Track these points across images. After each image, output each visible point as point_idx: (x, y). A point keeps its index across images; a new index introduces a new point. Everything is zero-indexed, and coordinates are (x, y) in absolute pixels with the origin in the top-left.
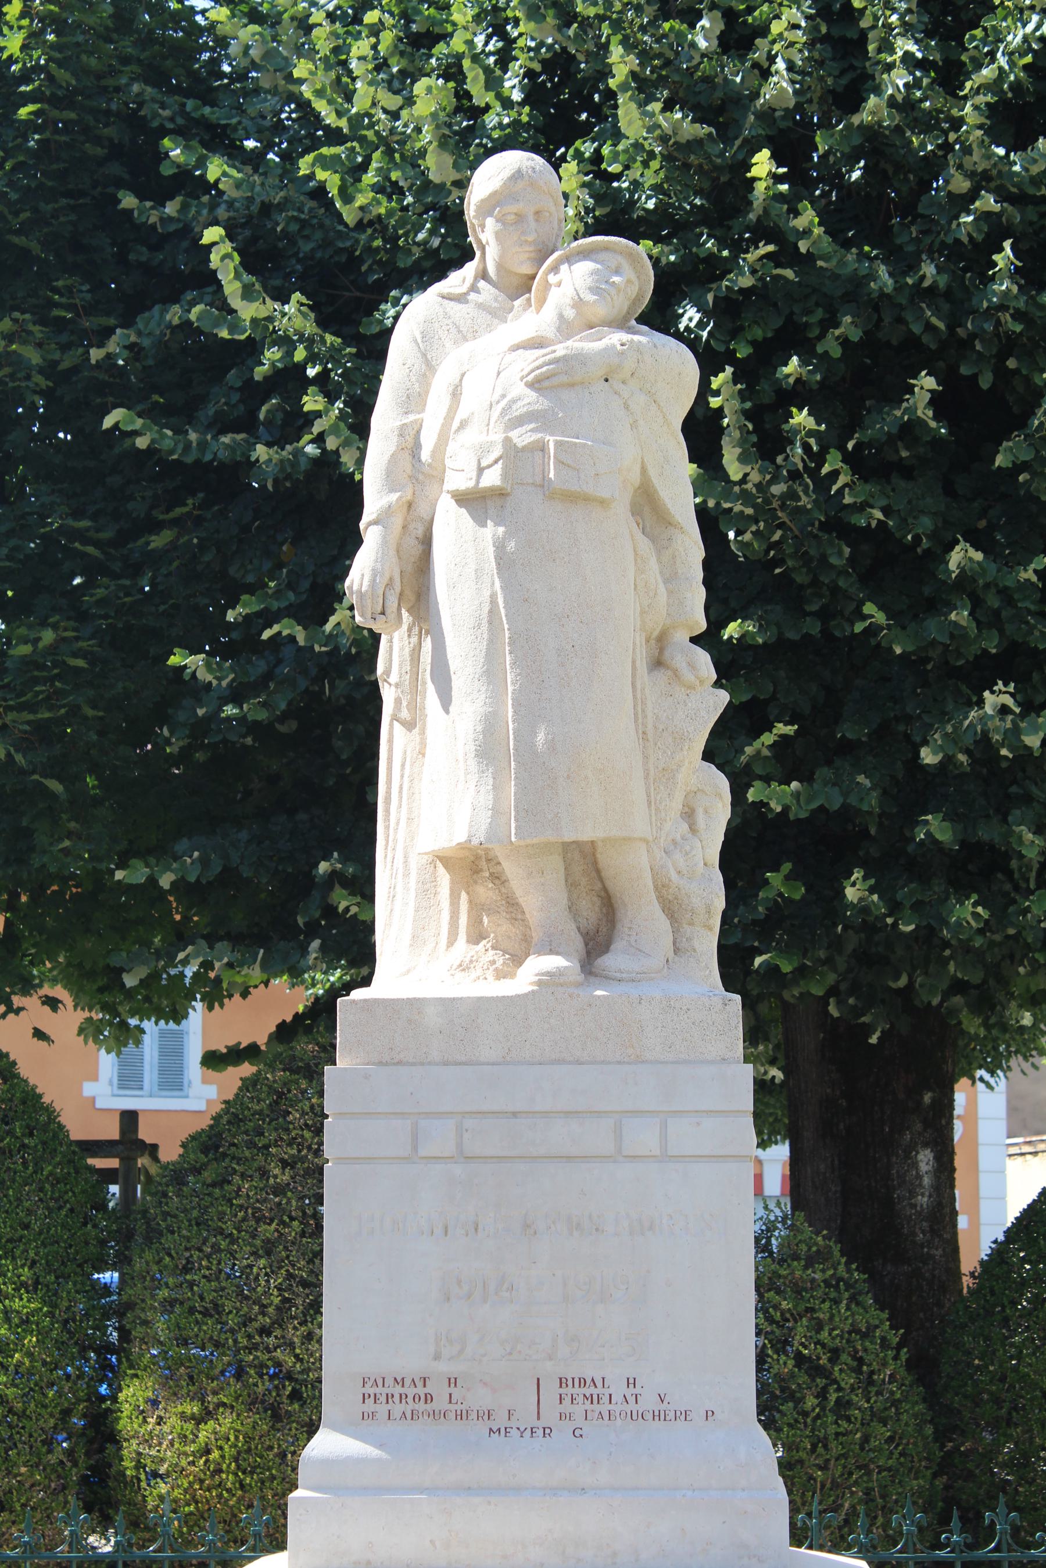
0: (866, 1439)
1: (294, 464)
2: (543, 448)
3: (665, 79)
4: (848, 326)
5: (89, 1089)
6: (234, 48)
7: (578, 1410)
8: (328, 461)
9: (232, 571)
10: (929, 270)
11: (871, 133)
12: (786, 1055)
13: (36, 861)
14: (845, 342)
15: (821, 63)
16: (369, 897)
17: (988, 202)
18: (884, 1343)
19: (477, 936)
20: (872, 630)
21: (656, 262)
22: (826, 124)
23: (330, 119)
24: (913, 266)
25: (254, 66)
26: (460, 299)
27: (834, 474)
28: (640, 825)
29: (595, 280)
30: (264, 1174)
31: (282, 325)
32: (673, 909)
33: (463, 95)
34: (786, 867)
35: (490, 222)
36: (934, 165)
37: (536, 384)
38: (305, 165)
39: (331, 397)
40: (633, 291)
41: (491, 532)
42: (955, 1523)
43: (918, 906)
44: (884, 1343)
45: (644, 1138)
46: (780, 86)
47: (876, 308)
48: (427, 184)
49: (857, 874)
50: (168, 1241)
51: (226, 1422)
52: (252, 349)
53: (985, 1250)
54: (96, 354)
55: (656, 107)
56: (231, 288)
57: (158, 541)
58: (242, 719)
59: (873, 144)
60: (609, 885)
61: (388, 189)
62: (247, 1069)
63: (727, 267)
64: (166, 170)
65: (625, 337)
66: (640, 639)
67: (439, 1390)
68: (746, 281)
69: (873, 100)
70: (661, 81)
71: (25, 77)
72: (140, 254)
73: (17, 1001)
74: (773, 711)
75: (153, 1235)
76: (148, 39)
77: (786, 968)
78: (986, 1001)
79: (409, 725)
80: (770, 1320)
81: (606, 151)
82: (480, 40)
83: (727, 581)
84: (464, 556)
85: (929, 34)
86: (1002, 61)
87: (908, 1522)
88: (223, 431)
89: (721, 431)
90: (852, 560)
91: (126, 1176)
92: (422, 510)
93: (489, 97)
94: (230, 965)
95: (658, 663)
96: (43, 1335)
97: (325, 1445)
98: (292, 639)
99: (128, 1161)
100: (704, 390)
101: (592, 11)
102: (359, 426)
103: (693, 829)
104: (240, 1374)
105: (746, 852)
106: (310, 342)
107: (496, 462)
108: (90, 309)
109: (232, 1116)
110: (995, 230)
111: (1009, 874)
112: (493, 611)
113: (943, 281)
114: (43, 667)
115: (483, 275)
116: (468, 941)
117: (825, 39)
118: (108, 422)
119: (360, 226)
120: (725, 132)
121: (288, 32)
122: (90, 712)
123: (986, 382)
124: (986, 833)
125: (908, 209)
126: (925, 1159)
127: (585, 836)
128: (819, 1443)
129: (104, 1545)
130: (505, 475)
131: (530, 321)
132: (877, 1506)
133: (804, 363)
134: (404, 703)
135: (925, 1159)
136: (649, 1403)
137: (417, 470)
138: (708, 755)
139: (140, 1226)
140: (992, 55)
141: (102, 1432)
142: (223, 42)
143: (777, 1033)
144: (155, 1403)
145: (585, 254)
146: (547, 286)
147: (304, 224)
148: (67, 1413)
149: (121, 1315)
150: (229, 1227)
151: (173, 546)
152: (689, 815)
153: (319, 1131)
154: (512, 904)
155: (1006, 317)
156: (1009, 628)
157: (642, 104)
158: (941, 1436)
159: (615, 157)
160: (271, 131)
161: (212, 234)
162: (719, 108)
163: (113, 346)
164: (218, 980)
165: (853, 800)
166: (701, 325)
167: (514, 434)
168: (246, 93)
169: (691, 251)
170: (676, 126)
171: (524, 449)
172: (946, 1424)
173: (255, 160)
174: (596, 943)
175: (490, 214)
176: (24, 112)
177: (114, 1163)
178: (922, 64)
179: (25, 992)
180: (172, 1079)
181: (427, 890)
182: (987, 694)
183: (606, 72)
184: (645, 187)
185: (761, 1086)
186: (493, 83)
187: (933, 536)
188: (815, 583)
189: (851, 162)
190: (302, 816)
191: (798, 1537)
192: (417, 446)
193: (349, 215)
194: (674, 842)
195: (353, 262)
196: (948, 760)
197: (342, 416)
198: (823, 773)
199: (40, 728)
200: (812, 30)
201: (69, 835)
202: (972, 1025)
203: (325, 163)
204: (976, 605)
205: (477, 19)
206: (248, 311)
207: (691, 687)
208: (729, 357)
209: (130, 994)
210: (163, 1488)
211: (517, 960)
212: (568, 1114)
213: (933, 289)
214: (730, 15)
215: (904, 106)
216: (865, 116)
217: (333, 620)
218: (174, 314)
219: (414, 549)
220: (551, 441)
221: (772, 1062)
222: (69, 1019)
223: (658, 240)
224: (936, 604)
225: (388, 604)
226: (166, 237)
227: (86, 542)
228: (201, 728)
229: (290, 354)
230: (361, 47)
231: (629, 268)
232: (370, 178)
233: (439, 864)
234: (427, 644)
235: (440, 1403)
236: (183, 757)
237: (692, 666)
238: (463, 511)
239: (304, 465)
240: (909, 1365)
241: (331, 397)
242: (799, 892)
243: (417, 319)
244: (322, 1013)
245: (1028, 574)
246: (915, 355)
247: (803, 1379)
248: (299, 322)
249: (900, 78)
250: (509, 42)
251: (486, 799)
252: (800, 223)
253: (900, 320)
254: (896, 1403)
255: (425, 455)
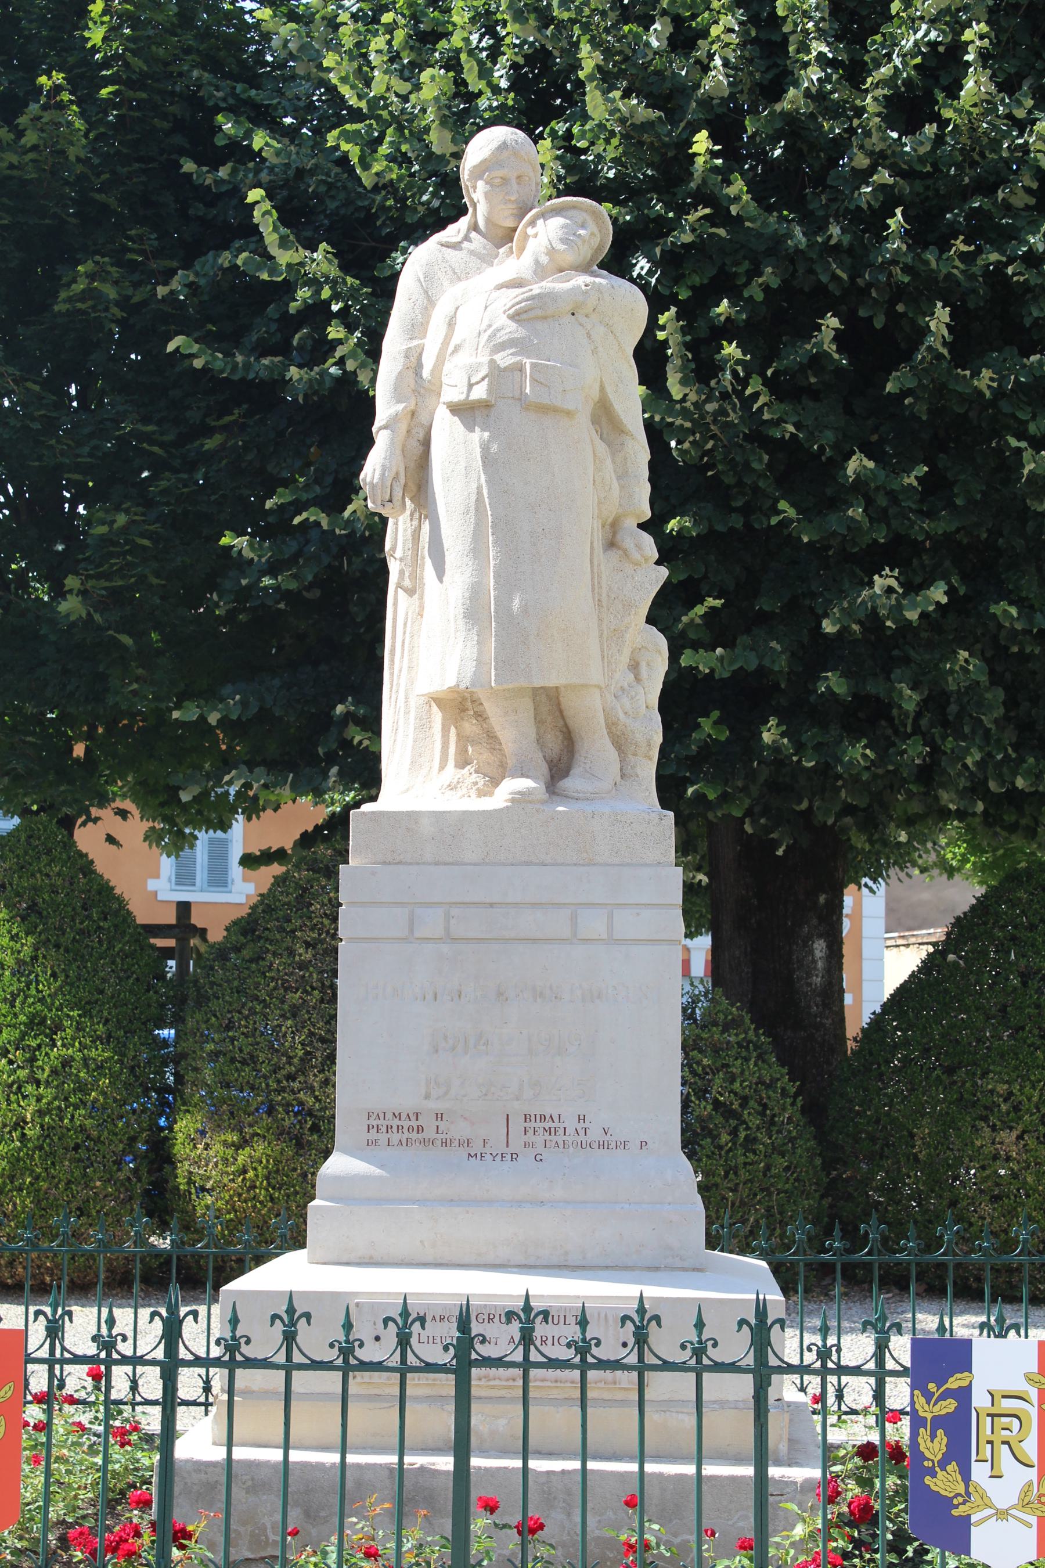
0: (768, 1168)
1: (321, 382)
2: (520, 368)
3: (624, 72)
4: (769, 276)
5: (152, 885)
6: (276, 42)
7: (539, 1140)
8: (348, 380)
9: (270, 468)
10: (835, 230)
11: (790, 118)
12: (711, 864)
13: (111, 700)
14: (766, 288)
15: (750, 61)
16: (377, 733)
17: (883, 176)
18: (784, 1092)
19: (463, 762)
20: (785, 523)
21: (615, 221)
22: (754, 111)
23: (353, 101)
24: (823, 228)
25: (292, 56)
26: (455, 246)
27: (756, 395)
28: (595, 675)
29: (563, 233)
30: (291, 953)
31: (311, 269)
32: (620, 742)
33: (460, 82)
34: (715, 714)
35: (480, 184)
36: (840, 146)
37: (516, 317)
38: (332, 138)
39: (351, 329)
40: (597, 241)
41: (478, 436)
42: (837, 1232)
43: (818, 747)
44: (784, 1092)
45: (594, 925)
46: (717, 79)
47: (792, 261)
48: (431, 155)
49: (773, 722)
50: (214, 1005)
51: (260, 1148)
52: (287, 288)
53: (866, 1019)
54: (161, 291)
55: (617, 94)
56: (271, 239)
57: (210, 444)
58: (277, 588)
59: (792, 127)
60: (568, 721)
61: (398, 158)
62: (277, 869)
63: (673, 226)
64: (220, 141)
65: (588, 279)
66: (597, 524)
67: (428, 1122)
68: (687, 238)
69: (792, 92)
70: (621, 74)
71: (106, 64)
72: (198, 209)
73: (95, 812)
74: (704, 588)
75: (202, 1000)
76: (206, 34)
77: (712, 796)
78: (871, 820)
79: (411, 592)
80: (694, 1073)
81: (575, 130)
82: (474, 38)
83: (669, 482)
84: (456, 455)
85: (838, 38)
86: (897, 61)
87: (799, 1231)
88: (264, 355)
89: (666, 359)
90: (770, 466)
91: (181, 954)
92: (423, 418)
93: (482, 85)
94: (266, 786)
95: (611, 544)
96: (114, 1077)
97: (337, 1165)
98: (317, 524)
99: (182, 941)
100: (652, 325)
101: (566, 16)
102: (374, 353)
103: (638, 679)
104: (271, 1111)
105: (680, 700)
106: (334, 283)
107: (483, 379)
108: (157, 254)
109: (265, 907)
110: (888, 199)
111: (891, 719)
112: (479, 500)
113: (846, 240)
114: (116, 544)
115: (475, 227)
116: (456, 767)
117: (754, 41)
118: (171, 347)
119: (376, 188)
120: (672, 115)
121: (320, 29)
122: (155, 581)
123: (879, 323)
124: (872, 688)
125: (819, 181)
126: (819, 948)
127: (552, 682)
128: (731, 1170)
129: (163, 1243)
130: (490, 390)
131: (512, 265)
132: (776, 1220)
133: (732, 304)
134: (407, 574)
135: (819, 948)
136: (595, 1134)
137: (419, 385)
138: (650, 620)
139: (192, 993)
140: (889, 56)
141: (160, 1155)
142: (266, 37)
143: (703, 846)
144: (203, 1133)
145: (557, 211)
146: (526, 237)
147: (331, 186)
148: (133, 1140)
149: (177, 1063)
150: (263, 995)
151: (223, 447)
152: (634, 667)
153: (335, 919)
154: (491, 737)
155: (897, 270)
156: (895, 523)
157: (605, 92)
158: (827, 1167)
159: (583, 135)
160: (305, 110)
161: (254, 195)
162: (669, 97)
163: (175, 284)
164: (256, 798)
165: (767, 662)
166: (650, 273)
167: (498, 357)
168: (285, 79)
169: (644, 213)
170: (632, 111)
171: (506, 369)
172: (832, 1156)
173: (292, 133)
174: (558, 770)
175: (481, 178)
176: (104, 92)
177: (171, 943)
178: (833, 63)
179: (101, 806)
180: (219, 878)
181: (423, 725)
182: (876, 577)
183: (577, 66)
184: (607, 158)
185: (690, 889)
186: (484, 73)
187: (835, 447)
188: (740, 483)
189: (774, 142)
190: (323, 667)
191: (712, 1242)
192: (419, 365)
193: (367, 179)
194: (622, 689)
195: (370, 218)
196: (844, 630)
197: (360, 343)
198: (744, 640)
199: (114, 593)
200: (744, 34)
201: (137, 680)
202: (859, 841)
203: (348, 137)
204: (869, 504)
205: (473, 20)
206: (284, 258)
207: (637, 564)
208: (673, 300)
209: (184, 807)
210: (209, 1200)
211: (495, 782)
212: (534, 905)
213: (838, 246)
214: (678, 21)
215: (817, 96)
216: (785, 105)
217: (350, 508)
218: (225, 259)
219: (417, 450)
220: (528, 363)
221: (699, 869)
222: (135, 828)
223: (616, 203)
224: (836, 503)
225: (395, 493)
226: (219, 196)
227: (152, 443)
228: (243, 595)
229: (318, 292)
230: (378, 43)
231: (593, 223)
232: (384, 149)
233: (433, 704)
234: (426, 527)
235: (430, 1133)
236: (230, 617)
237: (639, 547)
238: (456, 419)
239: (328, 383)
240: (804, 1111)
241: (351, 329)
242: (724, 735)
243: (418, 264)
244: (339, 824)
245: (911, 480)
246: (823, 300)
247: (719, 1120)
248: (325, 267)
249: (815, 74)
250: (499, 40)
251: (472, 652)
252: (732, 191)
253: (811, 271)
254: (792, 1140)
255: (426, 373)
